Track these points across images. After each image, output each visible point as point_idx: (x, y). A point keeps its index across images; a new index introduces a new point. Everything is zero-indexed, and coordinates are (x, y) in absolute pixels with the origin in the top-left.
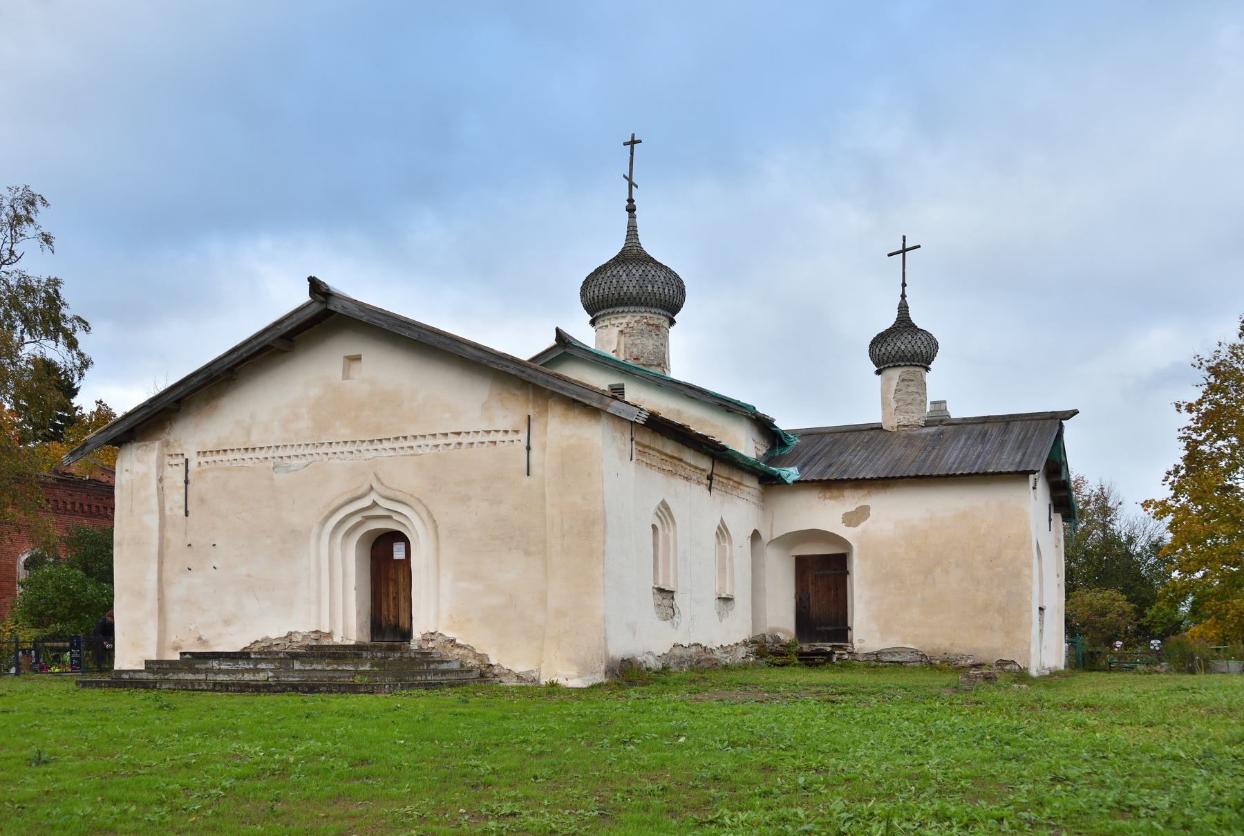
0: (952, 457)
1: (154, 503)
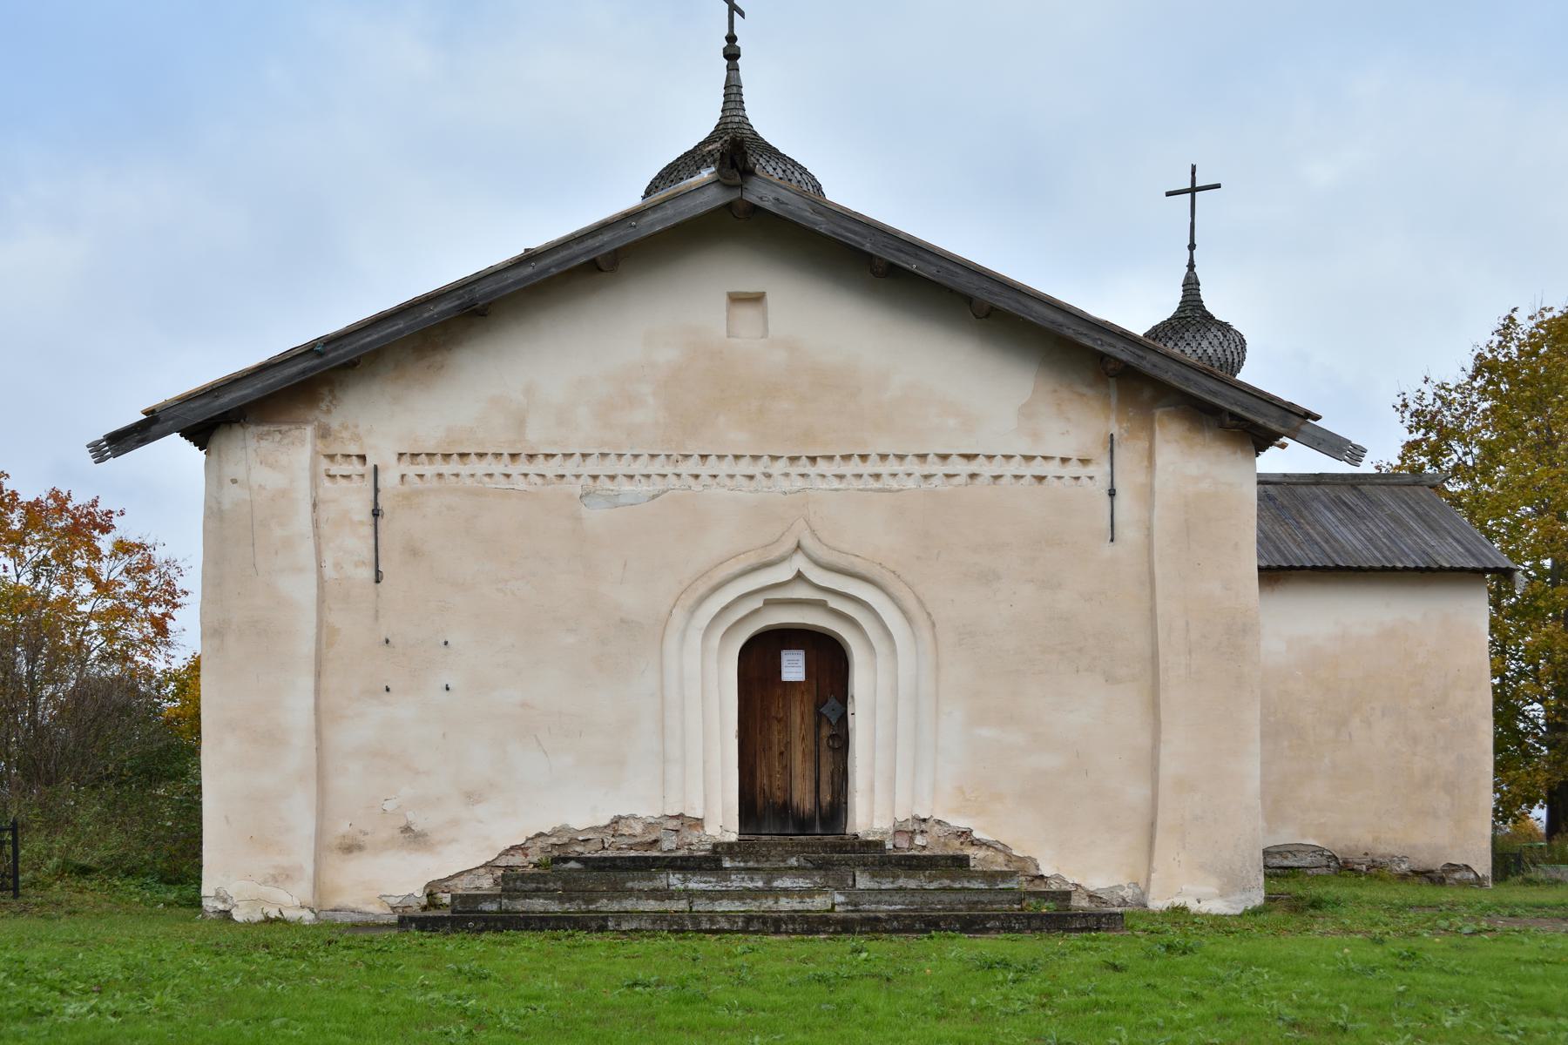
1: (307, 549)
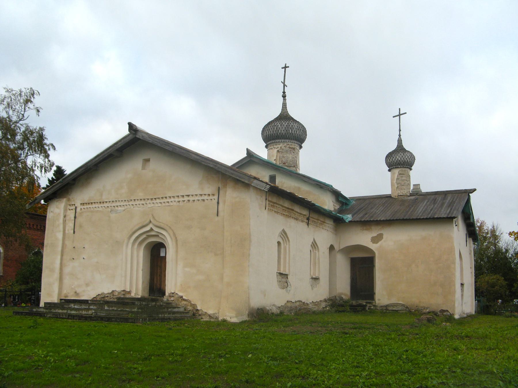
0: (420, 211)
1: (61, 227)
